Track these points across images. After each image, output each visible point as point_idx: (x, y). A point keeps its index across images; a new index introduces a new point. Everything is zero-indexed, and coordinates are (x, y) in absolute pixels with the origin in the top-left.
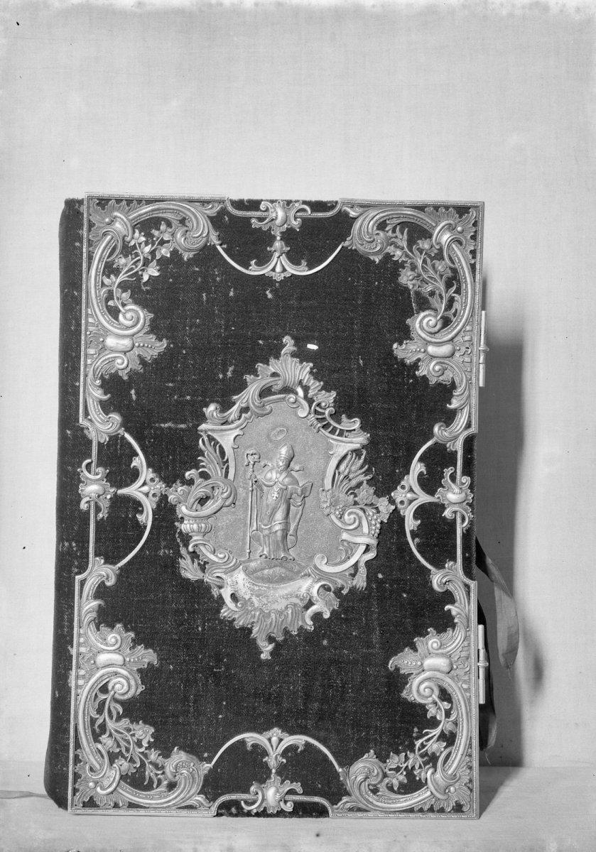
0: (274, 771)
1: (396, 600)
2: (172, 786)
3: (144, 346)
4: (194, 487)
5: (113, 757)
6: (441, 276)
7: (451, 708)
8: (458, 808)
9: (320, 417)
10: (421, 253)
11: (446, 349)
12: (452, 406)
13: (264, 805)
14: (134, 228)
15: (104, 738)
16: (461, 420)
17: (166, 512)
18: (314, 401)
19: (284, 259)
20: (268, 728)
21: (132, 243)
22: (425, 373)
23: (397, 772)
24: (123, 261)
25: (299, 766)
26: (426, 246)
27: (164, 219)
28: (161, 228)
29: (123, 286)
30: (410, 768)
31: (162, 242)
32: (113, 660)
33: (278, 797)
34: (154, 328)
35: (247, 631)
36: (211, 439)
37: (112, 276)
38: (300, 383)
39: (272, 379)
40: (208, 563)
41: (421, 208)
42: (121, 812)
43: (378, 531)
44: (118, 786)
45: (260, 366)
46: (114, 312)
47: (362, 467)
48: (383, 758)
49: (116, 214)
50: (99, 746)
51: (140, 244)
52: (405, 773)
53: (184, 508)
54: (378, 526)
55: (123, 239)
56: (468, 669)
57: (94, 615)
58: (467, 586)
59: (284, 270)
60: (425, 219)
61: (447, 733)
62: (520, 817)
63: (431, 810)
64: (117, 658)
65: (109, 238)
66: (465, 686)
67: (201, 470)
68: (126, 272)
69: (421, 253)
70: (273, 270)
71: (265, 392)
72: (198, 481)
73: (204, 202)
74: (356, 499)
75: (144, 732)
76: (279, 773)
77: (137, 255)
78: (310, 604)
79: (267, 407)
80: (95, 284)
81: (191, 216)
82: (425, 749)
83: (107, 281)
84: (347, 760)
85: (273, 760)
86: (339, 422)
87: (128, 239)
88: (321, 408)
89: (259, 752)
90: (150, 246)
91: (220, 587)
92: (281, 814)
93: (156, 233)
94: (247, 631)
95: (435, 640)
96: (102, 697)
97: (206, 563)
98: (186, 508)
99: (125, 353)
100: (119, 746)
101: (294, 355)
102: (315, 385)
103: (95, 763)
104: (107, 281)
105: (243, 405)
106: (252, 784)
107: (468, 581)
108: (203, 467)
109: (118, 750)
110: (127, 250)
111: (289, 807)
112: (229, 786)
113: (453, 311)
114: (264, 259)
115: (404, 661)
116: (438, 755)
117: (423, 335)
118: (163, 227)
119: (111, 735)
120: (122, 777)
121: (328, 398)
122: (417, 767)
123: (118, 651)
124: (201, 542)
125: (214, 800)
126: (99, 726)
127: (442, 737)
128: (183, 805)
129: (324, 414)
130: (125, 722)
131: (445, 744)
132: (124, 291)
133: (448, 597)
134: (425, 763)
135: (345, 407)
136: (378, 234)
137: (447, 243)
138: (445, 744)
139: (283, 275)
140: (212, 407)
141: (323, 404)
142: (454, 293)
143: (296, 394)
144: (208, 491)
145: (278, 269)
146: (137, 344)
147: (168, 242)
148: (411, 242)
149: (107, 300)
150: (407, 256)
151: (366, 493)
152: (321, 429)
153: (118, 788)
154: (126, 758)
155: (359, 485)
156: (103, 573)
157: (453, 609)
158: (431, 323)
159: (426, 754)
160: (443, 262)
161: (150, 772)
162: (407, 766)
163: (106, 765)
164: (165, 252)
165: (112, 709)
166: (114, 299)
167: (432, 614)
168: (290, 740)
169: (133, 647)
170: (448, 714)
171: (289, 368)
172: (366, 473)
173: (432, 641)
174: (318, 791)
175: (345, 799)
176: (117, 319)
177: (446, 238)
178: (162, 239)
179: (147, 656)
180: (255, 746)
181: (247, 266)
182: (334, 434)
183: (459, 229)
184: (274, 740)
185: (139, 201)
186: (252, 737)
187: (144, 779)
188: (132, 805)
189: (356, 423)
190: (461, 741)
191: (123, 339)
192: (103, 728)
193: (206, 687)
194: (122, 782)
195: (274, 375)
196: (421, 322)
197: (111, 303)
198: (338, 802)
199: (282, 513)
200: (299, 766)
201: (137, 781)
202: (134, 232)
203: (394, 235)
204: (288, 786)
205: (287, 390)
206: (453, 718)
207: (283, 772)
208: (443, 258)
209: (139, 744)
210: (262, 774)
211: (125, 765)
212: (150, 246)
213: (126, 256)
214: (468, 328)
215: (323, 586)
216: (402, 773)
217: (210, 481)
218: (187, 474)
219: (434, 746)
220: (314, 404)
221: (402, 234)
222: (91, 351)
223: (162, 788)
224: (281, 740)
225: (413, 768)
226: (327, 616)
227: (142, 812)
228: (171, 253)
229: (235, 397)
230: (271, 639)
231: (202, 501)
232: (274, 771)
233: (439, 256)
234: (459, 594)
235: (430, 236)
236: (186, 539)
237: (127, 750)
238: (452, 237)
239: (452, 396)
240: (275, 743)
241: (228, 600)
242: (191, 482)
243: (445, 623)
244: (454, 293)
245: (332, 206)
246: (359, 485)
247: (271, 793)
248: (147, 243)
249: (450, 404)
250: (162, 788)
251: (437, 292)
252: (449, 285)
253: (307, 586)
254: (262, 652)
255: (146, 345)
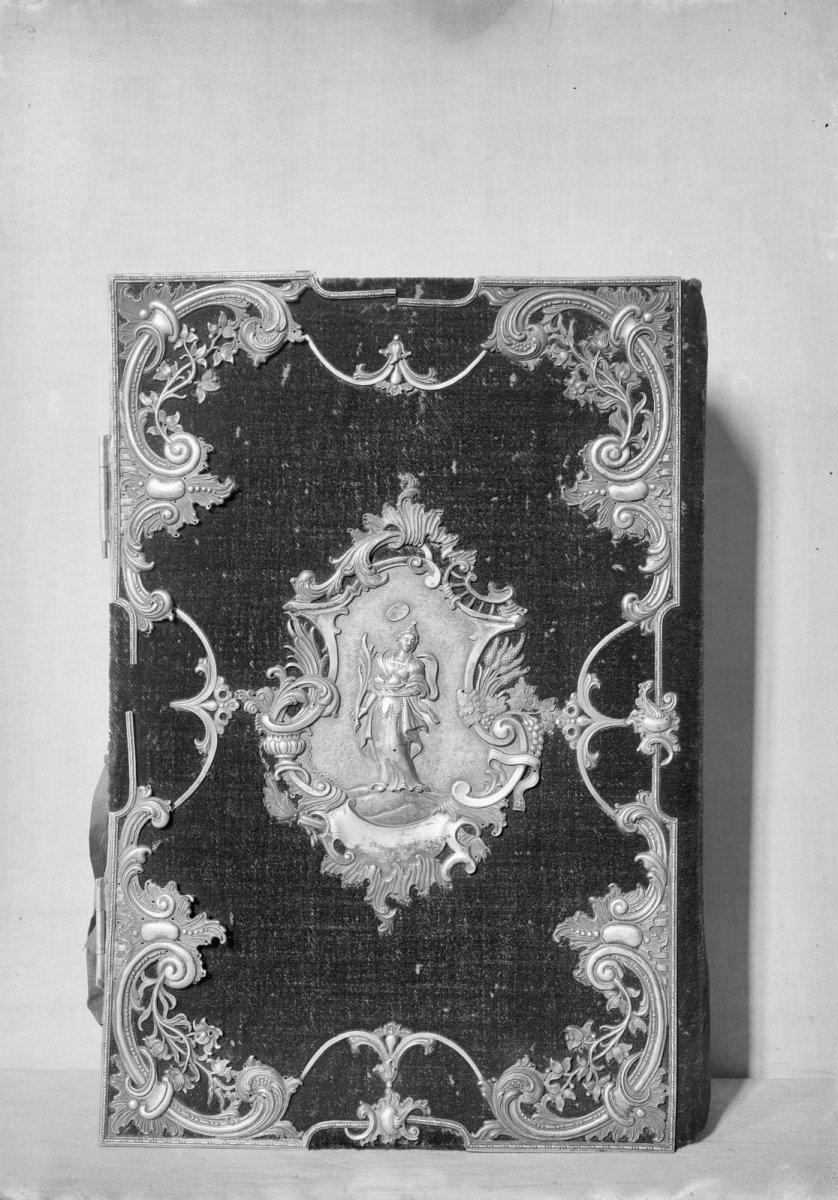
0: (389, 1085)
1: (556, 845)
2: (244, 1109)
3: (200, 490)
4: (277, 692)
5: (161, 1067)
6: (624, 386)
7: (640, 997)
8: (646, 1138)
9: (458, 585)
10: (594, 354)
11: (635, 489)
12: (646, 569)
13: (378, 1133)
14: (181, 322)
15: (151, 1039)
16: (660, 587)
17: (241, 726)
18: (448, 564)
19: (403, 366)
20: (380, 1023)
21: (179, 345)
22: (606, 525)
23: (562, 1084)
24: (167, 370)
25: (417, 1075)
26: (600, 344)
27: (222, 307)
28: (220, 320)
29: (169, 407)
30: (579, 1078)
31: (220, 341)
32: (174, 934)
33: (397, 1122)
34: (214, 464)
35: (359, 891)
36: (302, 619)
37: (153, 393)
38: (427, 540)
39: (388, 534)
40: (301, 796)
41: (591, 288)
42: (174, 1141)
43: (540, 747)
44: (169, 1106)
45: (369, 517)
46: (156, 444)
47: (517, 657)
48: (541, 1066)
49: (156, 304)
50: (144, 1050)
51: (189, 345)
52: (572, 1086)
53: (265, 719)
54: (541, 739)
55: (166, 341)
56: (665, 944)
57: (138, 868)
58: (663, 826)
59: (403, 381)
60: (596, 305)
61: (634, 1032)
62: (731, 1150)
63: (609, 1139)
64: (169, 929)
65: (146, 337)
66: (661, 967)
67: (289, 665)
68: (170, 388)
69: (594, 354)
70: (388, 379)
71: (375, 554)
72: (285, 681)
73: (277, 283)
74: (509, 702)
75: (206, 1034)
76: (395, 1088)
77: (186, 360)
78: (447, 851)
79: (382, 574)
80: (130, 403)
81: (260, 299)
82: (602, 1054)
83: (145, 400)
84: (494, 1070)
85: (387, 1071)
86: (485, 592)
87: (172, 339)
88: (458, 573)
89: (369, 1057)
90: (205, 347)
91: (319, 831)
92: (398, 1145)
93: (213, 328)
94: (359, 891)
95: (618, 901)
96: (148, 982)
97: (298, 797)
98: (270, 719)
99: (175, 500)
100: (170, 1052)
101: (415, 499)
102: (447, 542)
103: (137, 1074)
104: (145, 400)
105: (347, 573)
106: (359, 1105)
107: (666, 819)
108: (291, 660)
109: (169, 1058)
110: (172, 354)
111: (413, 1134)
112: (325, 1110)
113: (643, 434)
114: (375, 363)
115: (572, 930)
116: (620, 1062)
117: (602, 470)
118: (222, 318)
119: (159, 1036)
120: (175, 1094)
121: (466, 560)
122: (589, 1078)
123: (171, 918)
124: (291, 768)
125: (305, 1128)
126: (143, 1023)
127: (627, 1037)
128: (262, 1134)
129: (462, 581)
130: (181, 1019)
131: (630, 1047)
132: (170, 412)
133: (640, 843)
134: (601, 1074)
135: (489, 574)
136: (530, 330)
137: (631, 338)
138: (630, 1047)
139: (400, 388)
140: (305, 575)
141: (462, 568)
142: (644, 408)
143: (423, 555)
144: (298, 695)
145: (395, 378)
146: (190, 489)
147: (231, 339)
148: (579, 336)
149: (146, 426)
150: (574, 359)
151: (522, 692)
152: (460, 604)
153: (170, 1110)
154: (181, 1069)
155: (513, 683)
156: (150, 809)
157: (646, 858)
158: (612, 455)
159: (602, 1061)
160: (627, 366)
161: (215, 1087)
162: (575, 1076)
163: (153, 1078)
164: (224, 355)
165: (162, 999)
166: (155, 425)
167: (620, 862)
168: (411, 1039)
169: (192, 915)
170: (635, 1004)
171: (409, 517)
172: (522, 665)
173: (616, 902)
174: (451, 1111)
175: (488, 1125)
176: (162, 454)
177: (629, 329)
178: (221, 336)
179: (213, 929)
180: (363, 1048)
181: (350, 371)
182: (487, 613)
183: (647, 316)
184: (390, 1040)
185: (187, 284)
186: (359, 1036)
187: (206, 1094)
188: (188, 1134)
189: (509, 593)
190: (655, 1046)
191: (181, 479)
192: (149, 1024)
193: (278, 954)
194: (176, 1102)
195: (391, 527)
196: (599, 451)
197: (151, 430)
198: (478, 1129)
199: (404, 719)
200: (417, 1075)
201: (199, 1099)
202: (181, 329)
203: (556, 329)
204: (410, 1104)
205: (408, 550)
206: (642, 1012)
207: (404, 1090)
208: (625, 360)
209: (198, 1049)
210: (373, 1093)
211: (180, 1078)
212: (205, 347)
213: (171, 364)
214: (666, 458)
215: (464, 826)
216: (568, 1087)
217: (301, 682)
218: (270, 671)
219: (615, 1050)
220: (450, 567)
221: (567, 328)
222: (126, 500)
223: (232, 1111)
224: (399, 1040)
225: (583, 1079)
226: (471, 869)
227: (204, 1141)
228: (235, 356)
229: (335, 561)
230: (391, 903)
231: (292, 709)
232: (389, 1085)
233: (620, 357)
234: (655, 838)
235: (606, 327)
236: (273, 760)
237: (182, 1058)
238: (640, 328)
239: (647, 555)
240: (391, 1044)
241: (330, 848)
242: (274, 683)
243: (634, 878)
244: (644, 408)
245: (461, 287)
246: (513, 683)
247: (387, 1114)
248: (199, 344)
249: (644, 565)
250: (232, 1111)
251: (619, 407)
252: (635, 397)
253: (438, 828)
254: (380, 923)
255: (203, 489)
